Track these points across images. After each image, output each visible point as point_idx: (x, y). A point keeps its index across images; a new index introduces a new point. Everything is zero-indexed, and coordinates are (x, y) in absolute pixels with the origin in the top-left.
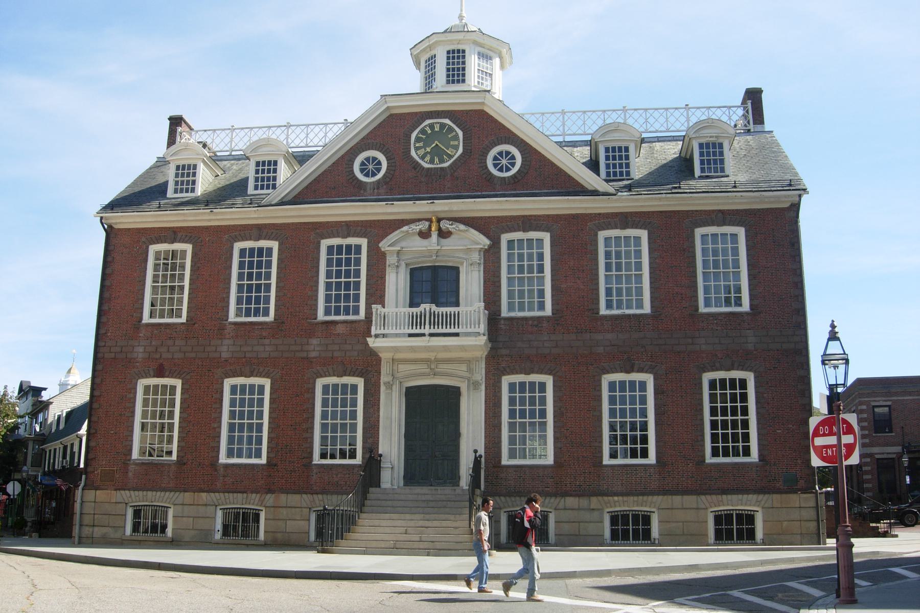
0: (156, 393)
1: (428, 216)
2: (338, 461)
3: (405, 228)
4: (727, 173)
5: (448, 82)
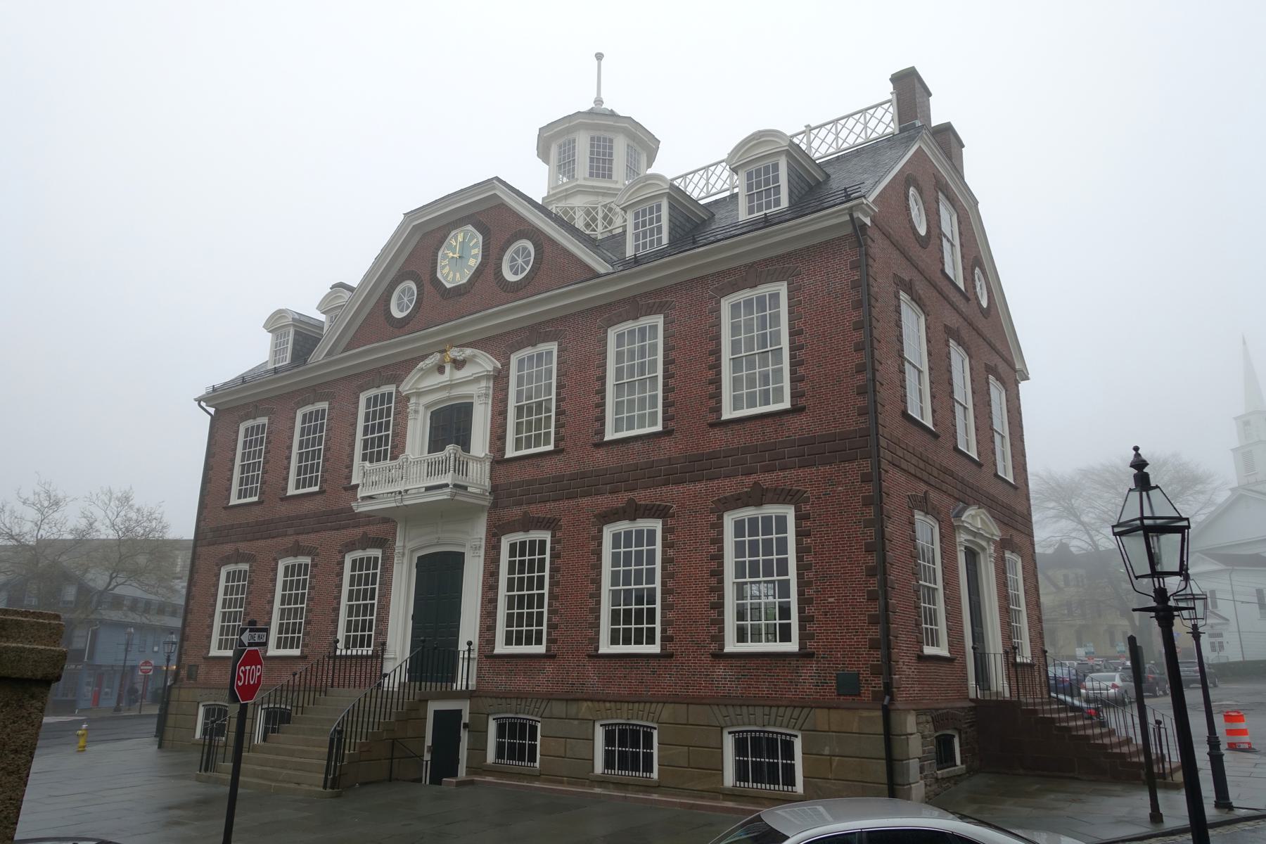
3: (421, 365)
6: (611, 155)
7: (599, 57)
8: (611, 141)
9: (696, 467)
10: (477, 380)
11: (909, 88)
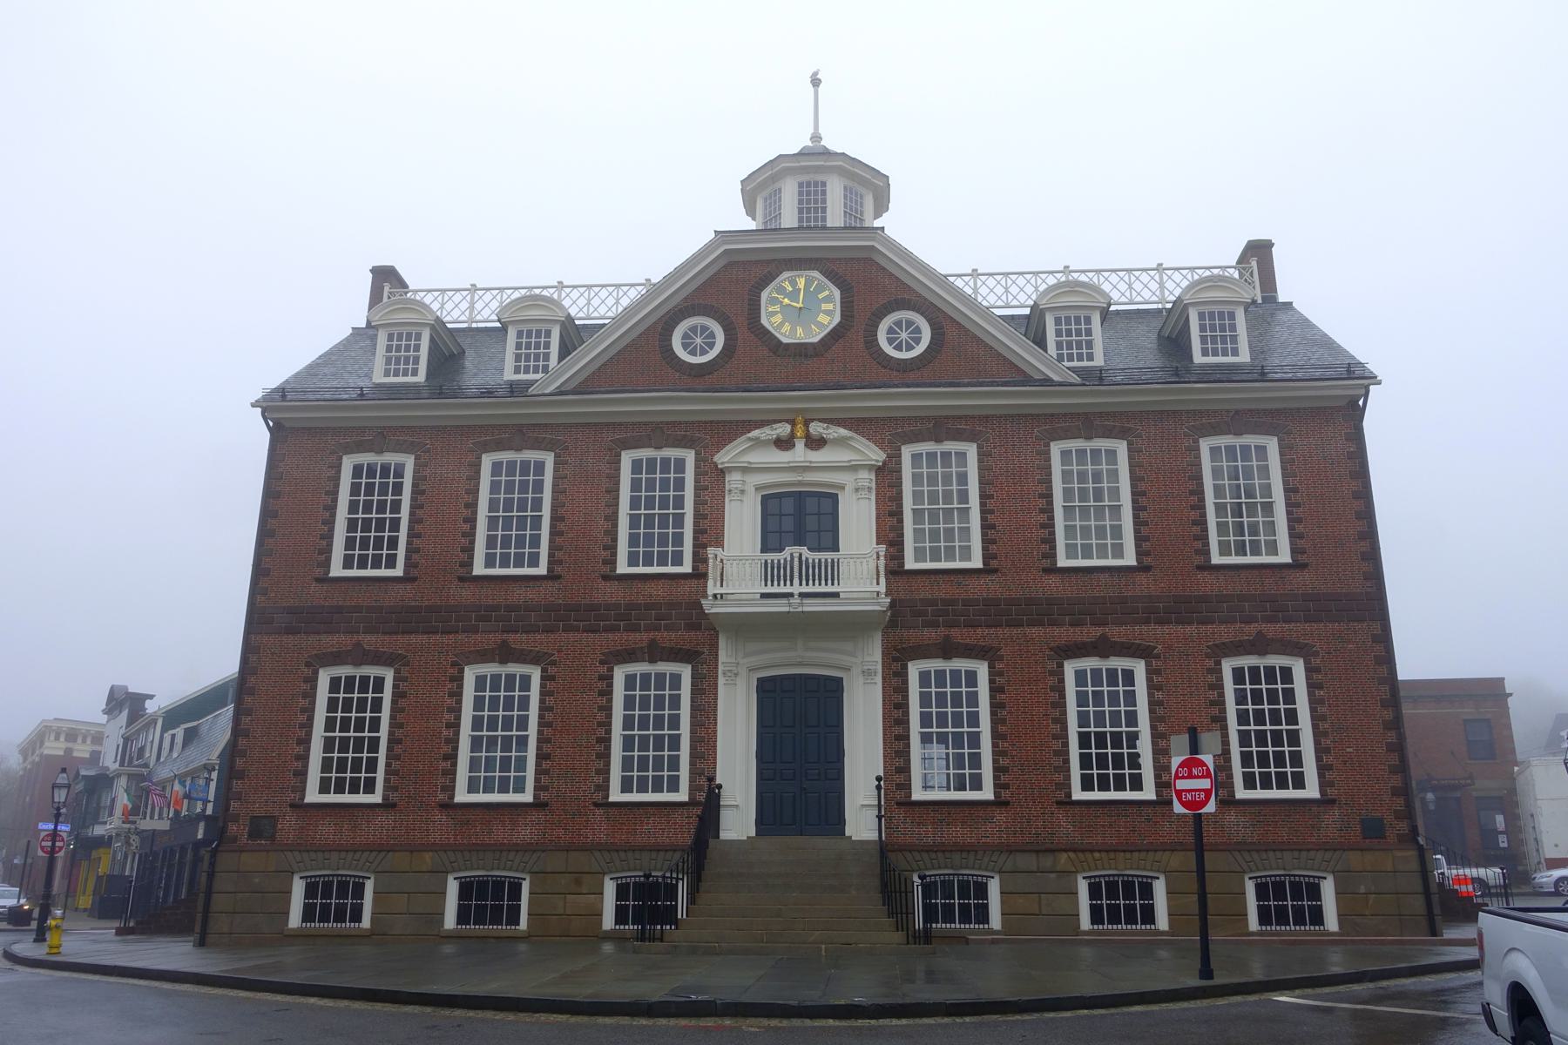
0: (349, 688)
2: (1274, 794)
3: (755, 433)
6: (824, 201)
7: (816, 82)
8: (824, 184)
9: (1182, 609)
10: (854, 468)
11: (1259, 253)
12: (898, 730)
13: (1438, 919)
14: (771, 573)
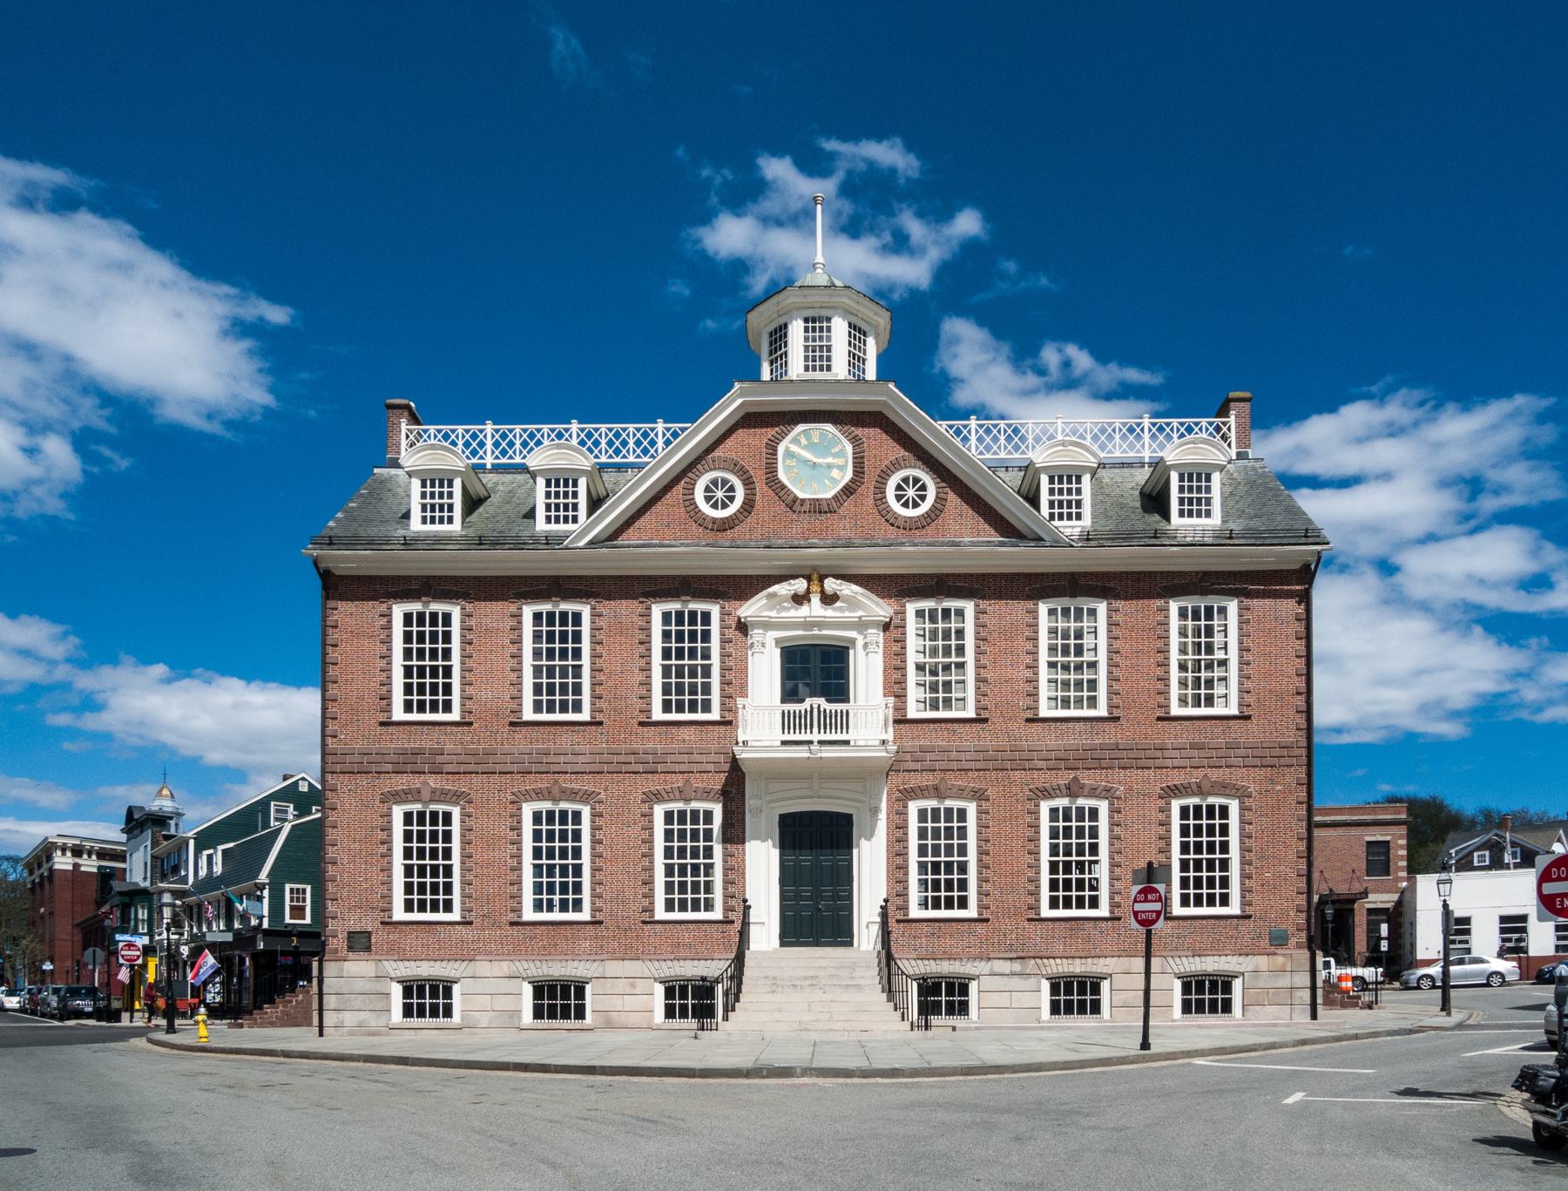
1: (808, 572)
4: (1475, 954)
5: (807, 369)
12: (899, 860)
13: (1320, 1008)
14: (788, 722)
